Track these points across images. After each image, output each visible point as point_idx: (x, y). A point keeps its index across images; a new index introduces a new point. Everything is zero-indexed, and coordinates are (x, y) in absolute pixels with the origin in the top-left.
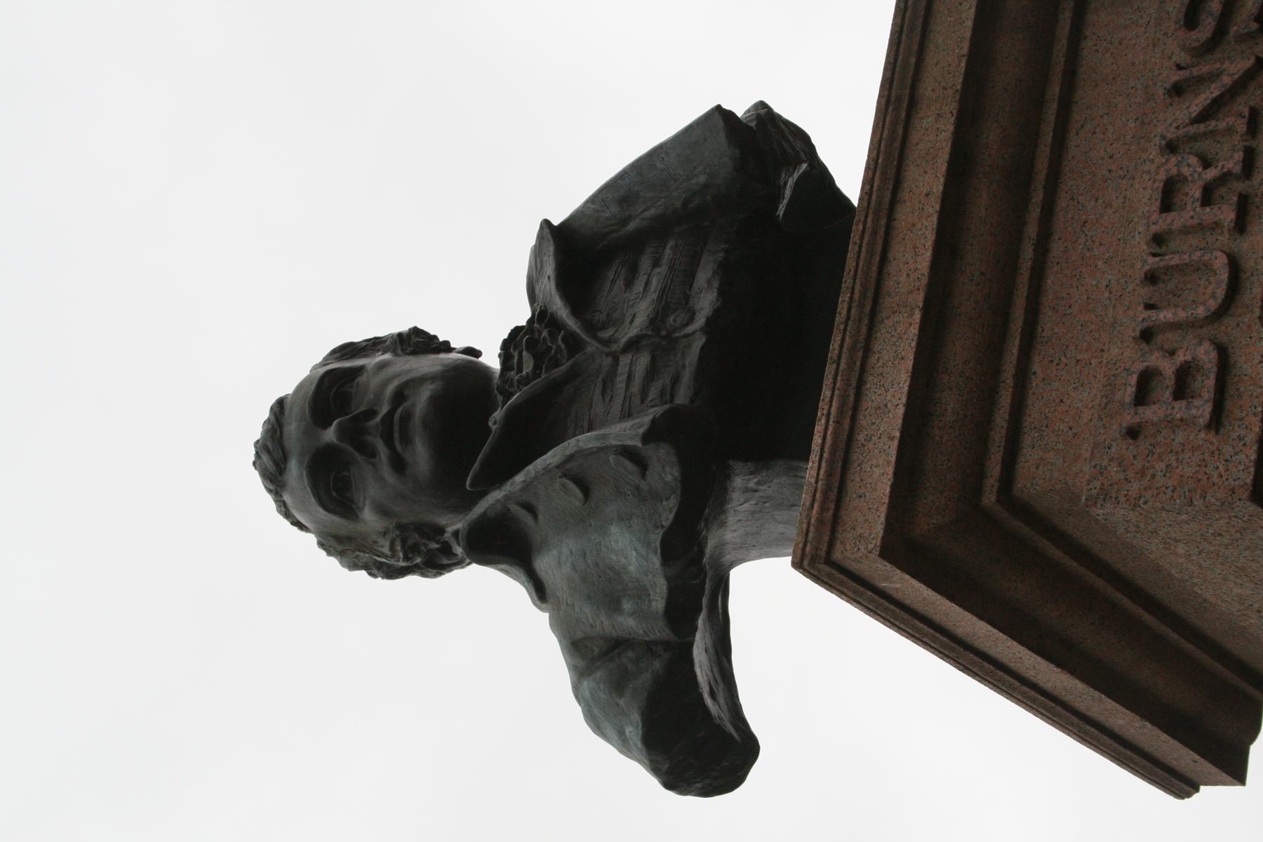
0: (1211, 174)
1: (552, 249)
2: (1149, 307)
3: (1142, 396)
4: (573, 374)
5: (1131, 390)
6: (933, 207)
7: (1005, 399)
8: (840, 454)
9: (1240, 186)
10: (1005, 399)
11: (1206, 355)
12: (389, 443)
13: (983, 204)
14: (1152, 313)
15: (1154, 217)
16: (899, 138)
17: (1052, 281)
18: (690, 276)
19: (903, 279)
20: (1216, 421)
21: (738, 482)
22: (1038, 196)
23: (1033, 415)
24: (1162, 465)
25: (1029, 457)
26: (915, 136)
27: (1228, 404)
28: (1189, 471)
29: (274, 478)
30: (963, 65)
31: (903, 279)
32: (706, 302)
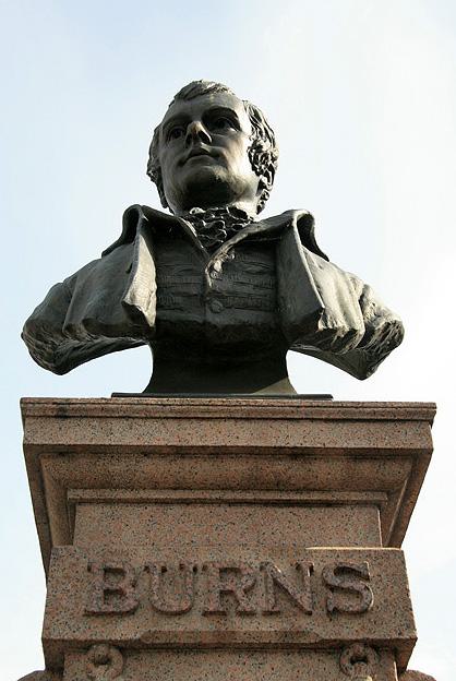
0: (239, 594)
1: (276, 225)
2: (164, 570)
3: (107, 571)
4: (199, 252)
5: (114, 565)
6: (273, 443)
7: (128, 495)
8: (85, 414)
9: (233, 610)
10: (128, 495)
11: (129, 603)
12: (191, 156)
13: (237, 469)
14: (159, 571)
15: (218, 565)
16: (274, 417)
17: (201, 510)
18: (246, 307)
19: (188, 431)
20: (89, 614)
21: (293, 319)
22: (249, 496)
23: (121, 510)
24: (69, 587)
25: (96, 512)
26: (276, 424)
27: (100, 620)
28: (64, 603)
29: (183, 96)
30: (319, 445)
31: (188, 431)
32: (220, 319)
